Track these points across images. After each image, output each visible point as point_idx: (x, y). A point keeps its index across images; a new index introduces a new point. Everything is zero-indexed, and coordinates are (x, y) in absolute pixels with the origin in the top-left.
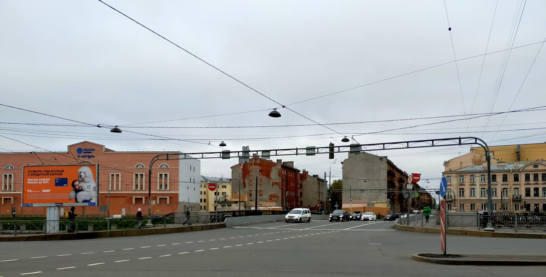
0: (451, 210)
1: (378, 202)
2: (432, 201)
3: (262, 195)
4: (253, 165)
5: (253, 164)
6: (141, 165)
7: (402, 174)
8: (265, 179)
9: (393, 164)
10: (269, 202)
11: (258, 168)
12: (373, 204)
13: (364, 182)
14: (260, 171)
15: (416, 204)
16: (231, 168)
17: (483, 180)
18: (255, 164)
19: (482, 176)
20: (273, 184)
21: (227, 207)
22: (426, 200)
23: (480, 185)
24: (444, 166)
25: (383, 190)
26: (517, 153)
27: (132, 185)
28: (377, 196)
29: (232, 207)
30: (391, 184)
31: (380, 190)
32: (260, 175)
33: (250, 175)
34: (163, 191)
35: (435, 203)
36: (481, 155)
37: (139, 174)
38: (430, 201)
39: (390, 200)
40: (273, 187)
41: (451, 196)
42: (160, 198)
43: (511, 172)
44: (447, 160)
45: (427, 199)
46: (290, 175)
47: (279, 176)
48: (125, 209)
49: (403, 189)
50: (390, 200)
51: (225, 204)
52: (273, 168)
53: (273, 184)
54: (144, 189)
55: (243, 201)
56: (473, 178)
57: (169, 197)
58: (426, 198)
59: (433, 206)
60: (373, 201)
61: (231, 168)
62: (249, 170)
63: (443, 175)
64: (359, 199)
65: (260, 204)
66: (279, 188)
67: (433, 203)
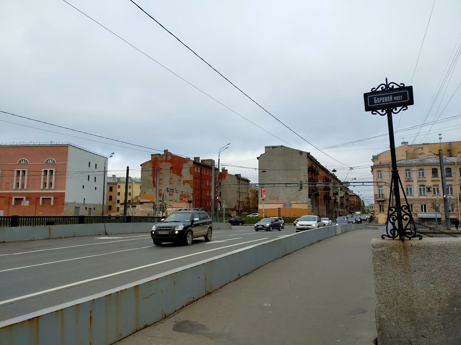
0: (383, 211)
1: (299, 202)
2: (361, 202)
3: (172, 195)
4: (164, 162)
5: (164, 161)
6: (24, 160)
7: (328, 174)
8: (176, 177)
9: (316, 160)
10: (180, 202)
11: (169, 165)
12: (290, 205)
13: (263, 172)
14: (171, 168)
15: (345, 205)
16: (141, 165)
17: (421, 175)
18: (166, 161)
19: (419, 170)
20: (184, 183)
21: (132, 209)
22: (355, 201)
23: (418, 181)
24: (372, 161)
25: (290, 184)
26: (449, 150)
27: (13, 183)
28: (297, 196)
29: (137, 208)
30: (312, 180)
31: (286, 184)
32: (170, 172)
33: (160, 173)
34: (47, 190)
35: (364, 204)
36: (415, 149)
37: (21, 170)
38: (359, 203)
39: (311, 200)
40: (184, 185)
41: (383, 195)
42: (43, 198)
43: (456, 164)
44: (376, 154)
45: (356, 201)
46: (206, 173)
47: (191, 173)
48: (3, 211)
49: (317, 182)
50: (311, 200)
51: (130, 205)
52: (185, 165)
53: (184, 183)
54: (25, 188)
55: (152, 202)
56: (409, 173)
57: (27, 197)
58: (355, 200)
59: (362, 208)
60: (293, 201)
61: (141, 165)
62: (159, 167)
63: (371, 170)
64: (277, 199)
65: (170, 205)
66: (190, 187)
67: (362, 205)
